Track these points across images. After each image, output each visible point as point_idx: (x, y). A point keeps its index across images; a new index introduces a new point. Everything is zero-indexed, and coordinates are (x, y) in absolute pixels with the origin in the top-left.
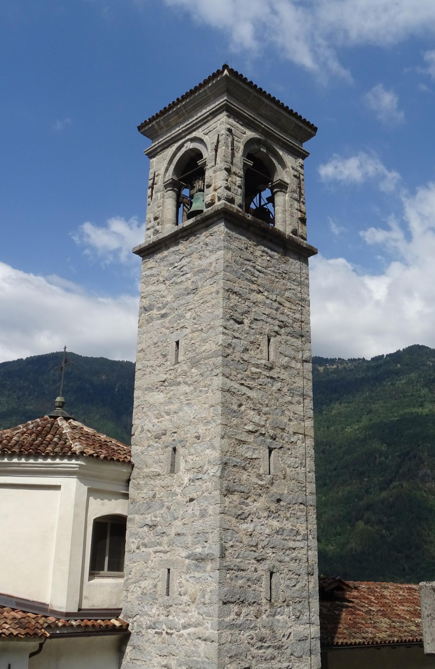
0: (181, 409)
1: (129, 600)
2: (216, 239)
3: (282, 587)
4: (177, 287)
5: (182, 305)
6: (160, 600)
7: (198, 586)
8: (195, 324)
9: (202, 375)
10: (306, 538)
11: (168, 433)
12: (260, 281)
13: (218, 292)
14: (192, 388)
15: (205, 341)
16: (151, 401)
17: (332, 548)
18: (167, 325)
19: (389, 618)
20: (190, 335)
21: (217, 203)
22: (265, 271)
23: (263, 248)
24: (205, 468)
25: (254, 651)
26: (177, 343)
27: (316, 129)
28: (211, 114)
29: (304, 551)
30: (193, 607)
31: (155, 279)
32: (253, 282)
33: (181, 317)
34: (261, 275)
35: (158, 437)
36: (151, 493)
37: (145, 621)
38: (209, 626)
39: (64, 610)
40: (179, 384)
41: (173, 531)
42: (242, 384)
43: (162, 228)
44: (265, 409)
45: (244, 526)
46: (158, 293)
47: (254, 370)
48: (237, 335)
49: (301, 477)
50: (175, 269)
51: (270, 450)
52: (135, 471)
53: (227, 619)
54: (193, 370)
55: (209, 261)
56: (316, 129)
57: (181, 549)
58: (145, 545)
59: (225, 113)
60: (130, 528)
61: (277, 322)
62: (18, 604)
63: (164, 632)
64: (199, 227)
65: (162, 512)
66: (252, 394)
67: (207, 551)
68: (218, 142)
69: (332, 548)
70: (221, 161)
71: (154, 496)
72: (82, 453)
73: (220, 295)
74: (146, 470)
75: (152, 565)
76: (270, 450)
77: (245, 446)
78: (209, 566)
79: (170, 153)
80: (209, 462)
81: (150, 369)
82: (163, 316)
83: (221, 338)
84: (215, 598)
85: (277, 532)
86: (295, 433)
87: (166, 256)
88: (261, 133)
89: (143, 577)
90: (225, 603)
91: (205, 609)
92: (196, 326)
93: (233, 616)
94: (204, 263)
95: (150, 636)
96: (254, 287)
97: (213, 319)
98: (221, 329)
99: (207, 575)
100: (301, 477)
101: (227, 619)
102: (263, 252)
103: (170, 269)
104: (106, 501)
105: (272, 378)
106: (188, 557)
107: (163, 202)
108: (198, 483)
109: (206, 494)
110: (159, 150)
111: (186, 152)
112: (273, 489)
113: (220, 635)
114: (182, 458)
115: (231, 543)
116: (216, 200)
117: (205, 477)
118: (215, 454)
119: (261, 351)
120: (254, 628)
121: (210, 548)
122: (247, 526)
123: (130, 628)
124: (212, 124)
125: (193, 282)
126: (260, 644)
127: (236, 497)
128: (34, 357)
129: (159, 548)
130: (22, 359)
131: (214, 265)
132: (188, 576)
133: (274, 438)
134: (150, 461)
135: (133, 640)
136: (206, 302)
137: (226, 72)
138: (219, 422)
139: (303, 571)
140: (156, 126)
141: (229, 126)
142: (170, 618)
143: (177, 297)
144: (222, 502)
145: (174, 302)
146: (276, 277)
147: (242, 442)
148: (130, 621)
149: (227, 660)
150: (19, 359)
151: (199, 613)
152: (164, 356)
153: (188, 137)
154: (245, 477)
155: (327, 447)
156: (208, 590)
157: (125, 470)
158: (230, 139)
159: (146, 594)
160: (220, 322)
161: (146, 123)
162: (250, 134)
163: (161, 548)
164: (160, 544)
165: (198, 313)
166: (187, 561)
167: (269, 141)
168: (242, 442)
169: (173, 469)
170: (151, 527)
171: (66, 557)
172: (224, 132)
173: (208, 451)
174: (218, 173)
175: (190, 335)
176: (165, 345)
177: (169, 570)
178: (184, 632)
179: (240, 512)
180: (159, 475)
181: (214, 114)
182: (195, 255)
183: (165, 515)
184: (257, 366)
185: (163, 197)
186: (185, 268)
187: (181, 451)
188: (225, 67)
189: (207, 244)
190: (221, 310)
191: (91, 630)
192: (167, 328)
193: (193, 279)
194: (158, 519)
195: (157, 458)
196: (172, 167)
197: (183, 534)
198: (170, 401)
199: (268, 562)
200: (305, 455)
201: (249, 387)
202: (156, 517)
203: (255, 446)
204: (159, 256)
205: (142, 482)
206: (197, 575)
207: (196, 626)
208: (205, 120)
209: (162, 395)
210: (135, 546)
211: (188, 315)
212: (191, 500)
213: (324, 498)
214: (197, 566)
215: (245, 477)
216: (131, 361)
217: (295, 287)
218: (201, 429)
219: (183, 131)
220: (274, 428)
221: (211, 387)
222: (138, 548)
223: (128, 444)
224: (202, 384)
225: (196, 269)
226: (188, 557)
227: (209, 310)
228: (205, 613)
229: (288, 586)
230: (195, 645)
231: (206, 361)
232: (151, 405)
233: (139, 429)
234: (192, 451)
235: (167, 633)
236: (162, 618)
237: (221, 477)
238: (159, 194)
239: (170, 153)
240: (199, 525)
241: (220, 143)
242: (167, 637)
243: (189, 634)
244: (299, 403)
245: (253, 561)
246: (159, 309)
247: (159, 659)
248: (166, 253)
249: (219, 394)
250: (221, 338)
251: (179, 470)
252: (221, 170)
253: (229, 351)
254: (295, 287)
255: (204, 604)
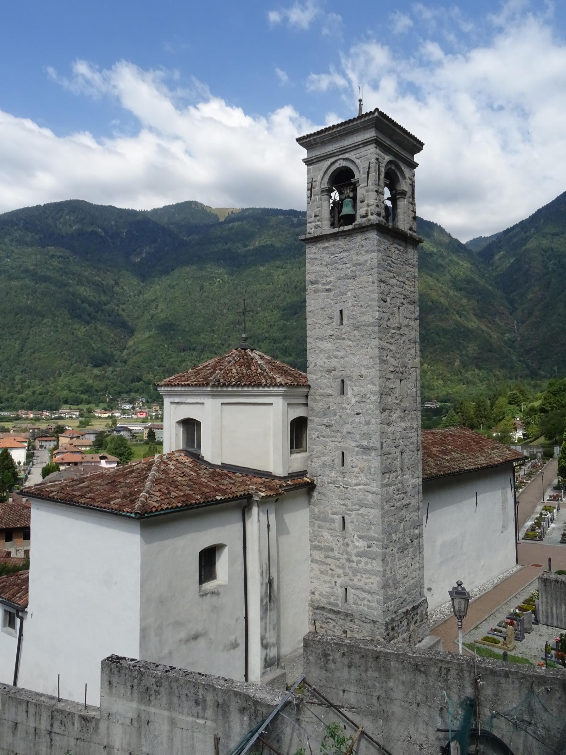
0: (346, 356)
1: (313, 466)
2: (370, 243)
3: (406, 460)
4: (338, 271)
5: (343, 285)
6: (337, 469)
7: (365, 464)
8: (355, 301)
9: (362, 336)
10: (416, 430)
11: (337, 370)
12: (394, 270)
13: (373, 283)
14: (355, 343)
15: (364, 314)
16: (322, 347)
17: (300, 360)
18: (332, 297)
19: (432, 458)
20: (352, 308)
21: (370, 217)
22: (397, 262)
23: (397, 246)
24: (368, 396)
25: (395, 496)
26: (341, 312)
27: (422, 144)
28: (362, 144)
29: (416, 438)
30: (362, 475)
31: (319, 262)
32: (390, 271)
33: (343, 293)
34: (395, 265)
35: (329, 371)
36: (326, 406)
37: (327, 479)
38: (375, 486)
39: (282, 476)
40: (344, 339)
41: (345, 431)
42: (388, 342)
43: (322, 224)
44: (398, 356)
45: (390, 429)
46: (322, 273)
47: (393, 331)
48: (384, 310)
49: (414, 395)
50: (336, 258)
51: (401, 381)
52: (312, 391)
53: (385, 482)
54: (355, 332)
55: (365, 258)
56: (422, 144)
57: (351, 442)
58: (324, 437)
59: (374, 145)
60: (310, 425)
61: (403, 296)
62: (255, 473)
63: (341, 487)
64: (356, 231)
65: (335, 418)
66: (392, 347)
67: (371, 445)
68: (369, 168)
69: (300, 360)
70: (372, 185)
71: (329, 408)
72: (286, 384)
73: (376, 284)
74: (321, 391)
75: (330, 448)
76: (401, 381)
77: (390, 381)
78: (373, 454)
79: (325, 165)
80: (371, 393)
81: (319, 326)
82: (328, 290)
83: (377, 314)
84: (379, 471)
85: (404, 430)
86: (411, 368)
87: (327, 247)
88: (393, 156)
89: (323, 454)
90: (383, 474)
91: (371, 477)
92: (356, 303)
93: (387, 480)
94: (361, 259)
95: (331, 488)
96: (392, 275)
97: (370, 300)
98: (377, 308)
99: (372, 458)
100: (414, 395)
101: (385, 482)
102: (396, 248)
103: (332, 257)
104: (296, 410)
105: (401, 334)
106: (357, 446)
107: (321, 204)
108: (363, 404)
109: (369, 411)
110: (315, 161)
111: (338, 168)
112: (402, 405)
113: (382, 491)
114: (349, 387)
115: (385, 440)
116: (369, 214)
117: (368, 401)
118: (376, 389)
119: (396, 318)
120: (395, 485)
121: (374, 443)
122: (391, 429)
123: (315, 483)
124: (363, 151)
125: (352, 271)
126: (398, 492)
127: (386, 413)
128: (51, 203)
129: (334, 439)
130: (40, 205)
131: (369, 262)
132: (357, 457)
133: (402, 373)
134: (324, 386)
135: (318, 488)
136: (364, 287)
137: (376, 114)
138: (378, 369)
139: (415, 449)
140: (312, 141)
141: (377, 156)
142: (345, 479)
143: (339, 279)
144: (381, 417)
145: (336, 282)
146: (402, 265)
147: (388, 379)
148: (315, 478)
149: (385, 503)
150: (37, 206)
151: (367, 478)
152: (331, 318)
153: (341, 157)
154: (390, 400)
155: (299, 284)
156: (373, 466)
157: (306, 390)
158: (377, 166)
159: (326, 465)
160: (375, 303)
161: (304, 138)
162: (388, 158)
163: (337, 439)
164: (335, 437)
165: (358, 294)
166: (356, 449)
167: (397, 161)
168: (388, 379)
169: (343, 392)
170: (327, 426)
171: (280, 446)
172: (373, 160)
173: (369, 386)
174: (370, 193)
175: (352, 308)
176: (331, 311)
177: (343, 453)
178: (357, 488)
179: (388, 422)
180: (331, 395)
181: (365, 144)
182: (352, 252)
183: (338, 420)
184: (394, 329)
185: (321, 200)
186: (344, 260)
187: (347, 382)
188: (377, 110)
189: (362, 246)
190: (377, 295)
191: (297, 486)
192: (332, 300)
193: (353, 269)
194: (333, 422)
195: (329, 384)
196: (327, 177)
197: (353, 433)
198: (337, 349)
199: (400, 447)
200: (416, 380)
201: (391, 344)
202: (331, 421)
203: (394, 380)
204: (320, 245)
205: (318, 398)
206: (364, 457)
207: (365, 485)
208: (356, 147)
209: (330, 344)
210: (316, 436)
211: (349, 293)
212: (358, 414)
213: (295, 323)
214: (363, 452)
215: (390, 400)
216: (135, 209)
217: (411, 269)
218: (364, 372)
219: (337, 152)
220: (402, 367)
221: (370, 345)
222: (318, 437)
223: (305, 371)
224: (363, 342)
225: (355, 262)
226: (357, 446)
227: (368, 294)
228: (371, 479)
229: (409, 459)
230: (364, 495)
231: (366, 328)
232: (322, 351)
233: (313, 364)
234: (357, 384)
235: (343, 487)
236: (339, 479)
237: (380, 403)
238: (317, 197)
239: (325, 165)
240: (365, 429)
241: (371, 169)
242: (343, 489)
243: (360, 489)
244: (413, 348)
245: (394, 448)
246: (324, 284)
247: (339, 501)
248: (327, 244)
249: (376, 351)
250: (377, 314)
251: (347, 394)
252: (372, 191)
253: (381, 322)
254: (411, 269)
255: (370, 474)
